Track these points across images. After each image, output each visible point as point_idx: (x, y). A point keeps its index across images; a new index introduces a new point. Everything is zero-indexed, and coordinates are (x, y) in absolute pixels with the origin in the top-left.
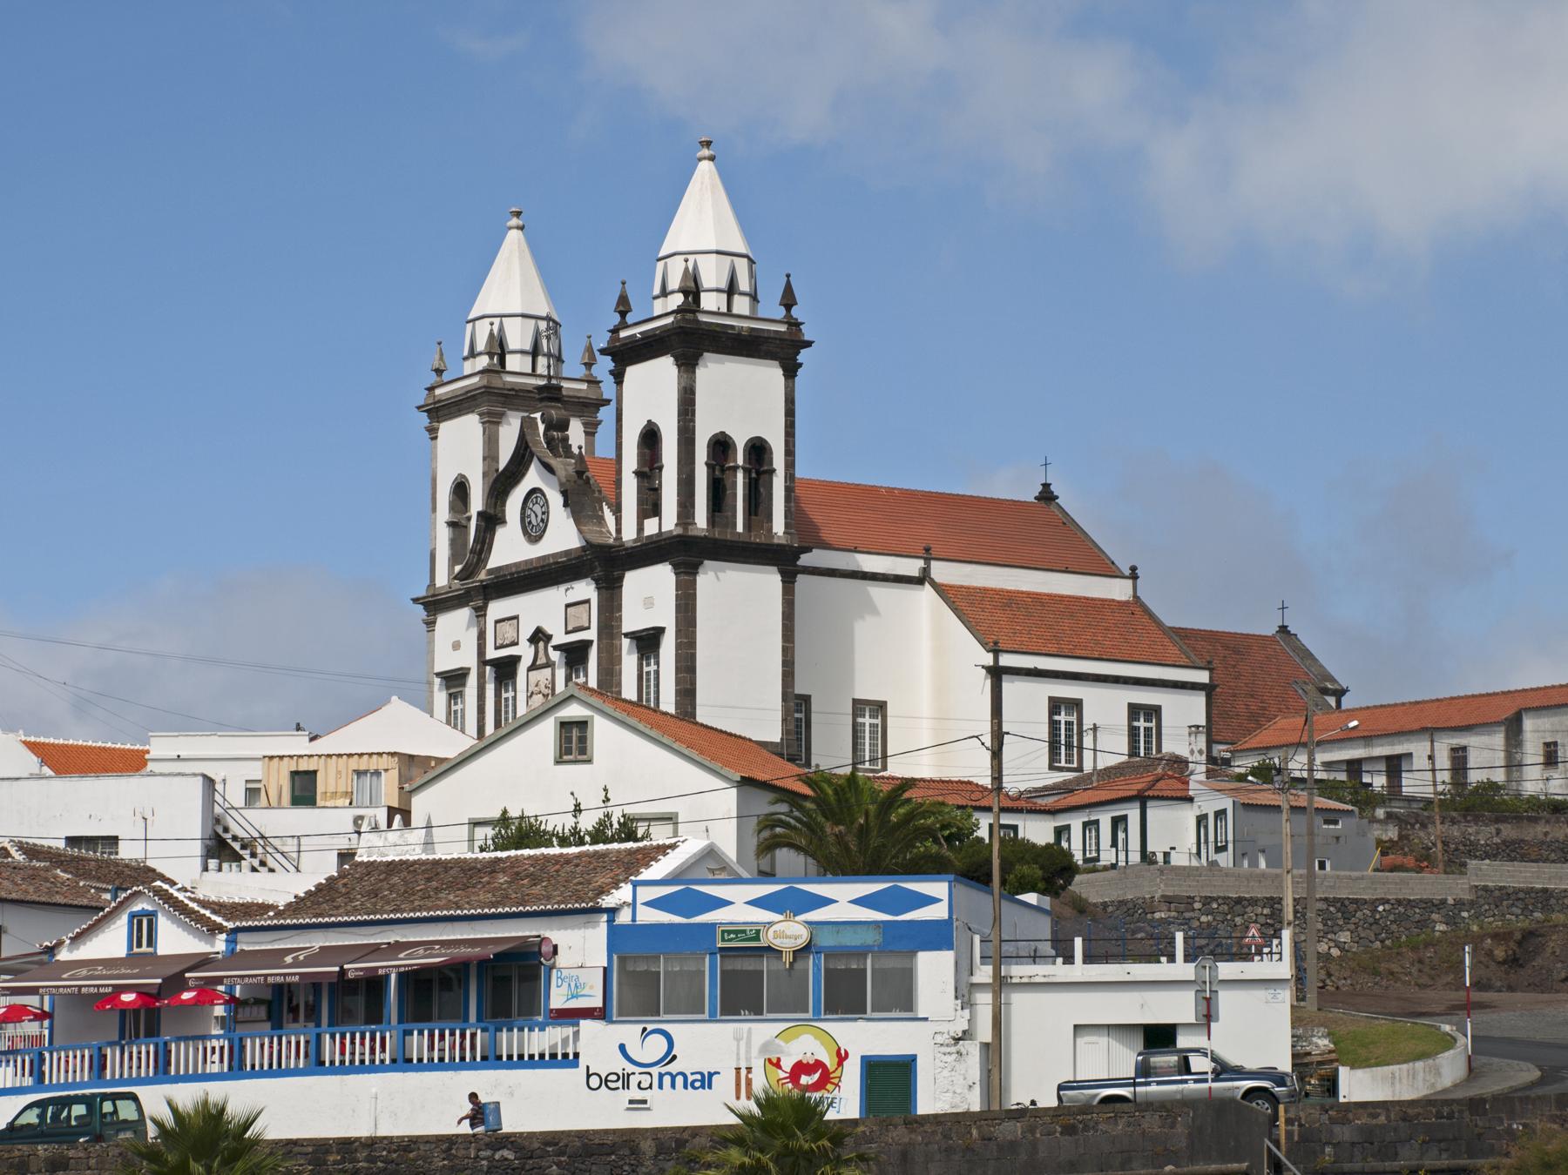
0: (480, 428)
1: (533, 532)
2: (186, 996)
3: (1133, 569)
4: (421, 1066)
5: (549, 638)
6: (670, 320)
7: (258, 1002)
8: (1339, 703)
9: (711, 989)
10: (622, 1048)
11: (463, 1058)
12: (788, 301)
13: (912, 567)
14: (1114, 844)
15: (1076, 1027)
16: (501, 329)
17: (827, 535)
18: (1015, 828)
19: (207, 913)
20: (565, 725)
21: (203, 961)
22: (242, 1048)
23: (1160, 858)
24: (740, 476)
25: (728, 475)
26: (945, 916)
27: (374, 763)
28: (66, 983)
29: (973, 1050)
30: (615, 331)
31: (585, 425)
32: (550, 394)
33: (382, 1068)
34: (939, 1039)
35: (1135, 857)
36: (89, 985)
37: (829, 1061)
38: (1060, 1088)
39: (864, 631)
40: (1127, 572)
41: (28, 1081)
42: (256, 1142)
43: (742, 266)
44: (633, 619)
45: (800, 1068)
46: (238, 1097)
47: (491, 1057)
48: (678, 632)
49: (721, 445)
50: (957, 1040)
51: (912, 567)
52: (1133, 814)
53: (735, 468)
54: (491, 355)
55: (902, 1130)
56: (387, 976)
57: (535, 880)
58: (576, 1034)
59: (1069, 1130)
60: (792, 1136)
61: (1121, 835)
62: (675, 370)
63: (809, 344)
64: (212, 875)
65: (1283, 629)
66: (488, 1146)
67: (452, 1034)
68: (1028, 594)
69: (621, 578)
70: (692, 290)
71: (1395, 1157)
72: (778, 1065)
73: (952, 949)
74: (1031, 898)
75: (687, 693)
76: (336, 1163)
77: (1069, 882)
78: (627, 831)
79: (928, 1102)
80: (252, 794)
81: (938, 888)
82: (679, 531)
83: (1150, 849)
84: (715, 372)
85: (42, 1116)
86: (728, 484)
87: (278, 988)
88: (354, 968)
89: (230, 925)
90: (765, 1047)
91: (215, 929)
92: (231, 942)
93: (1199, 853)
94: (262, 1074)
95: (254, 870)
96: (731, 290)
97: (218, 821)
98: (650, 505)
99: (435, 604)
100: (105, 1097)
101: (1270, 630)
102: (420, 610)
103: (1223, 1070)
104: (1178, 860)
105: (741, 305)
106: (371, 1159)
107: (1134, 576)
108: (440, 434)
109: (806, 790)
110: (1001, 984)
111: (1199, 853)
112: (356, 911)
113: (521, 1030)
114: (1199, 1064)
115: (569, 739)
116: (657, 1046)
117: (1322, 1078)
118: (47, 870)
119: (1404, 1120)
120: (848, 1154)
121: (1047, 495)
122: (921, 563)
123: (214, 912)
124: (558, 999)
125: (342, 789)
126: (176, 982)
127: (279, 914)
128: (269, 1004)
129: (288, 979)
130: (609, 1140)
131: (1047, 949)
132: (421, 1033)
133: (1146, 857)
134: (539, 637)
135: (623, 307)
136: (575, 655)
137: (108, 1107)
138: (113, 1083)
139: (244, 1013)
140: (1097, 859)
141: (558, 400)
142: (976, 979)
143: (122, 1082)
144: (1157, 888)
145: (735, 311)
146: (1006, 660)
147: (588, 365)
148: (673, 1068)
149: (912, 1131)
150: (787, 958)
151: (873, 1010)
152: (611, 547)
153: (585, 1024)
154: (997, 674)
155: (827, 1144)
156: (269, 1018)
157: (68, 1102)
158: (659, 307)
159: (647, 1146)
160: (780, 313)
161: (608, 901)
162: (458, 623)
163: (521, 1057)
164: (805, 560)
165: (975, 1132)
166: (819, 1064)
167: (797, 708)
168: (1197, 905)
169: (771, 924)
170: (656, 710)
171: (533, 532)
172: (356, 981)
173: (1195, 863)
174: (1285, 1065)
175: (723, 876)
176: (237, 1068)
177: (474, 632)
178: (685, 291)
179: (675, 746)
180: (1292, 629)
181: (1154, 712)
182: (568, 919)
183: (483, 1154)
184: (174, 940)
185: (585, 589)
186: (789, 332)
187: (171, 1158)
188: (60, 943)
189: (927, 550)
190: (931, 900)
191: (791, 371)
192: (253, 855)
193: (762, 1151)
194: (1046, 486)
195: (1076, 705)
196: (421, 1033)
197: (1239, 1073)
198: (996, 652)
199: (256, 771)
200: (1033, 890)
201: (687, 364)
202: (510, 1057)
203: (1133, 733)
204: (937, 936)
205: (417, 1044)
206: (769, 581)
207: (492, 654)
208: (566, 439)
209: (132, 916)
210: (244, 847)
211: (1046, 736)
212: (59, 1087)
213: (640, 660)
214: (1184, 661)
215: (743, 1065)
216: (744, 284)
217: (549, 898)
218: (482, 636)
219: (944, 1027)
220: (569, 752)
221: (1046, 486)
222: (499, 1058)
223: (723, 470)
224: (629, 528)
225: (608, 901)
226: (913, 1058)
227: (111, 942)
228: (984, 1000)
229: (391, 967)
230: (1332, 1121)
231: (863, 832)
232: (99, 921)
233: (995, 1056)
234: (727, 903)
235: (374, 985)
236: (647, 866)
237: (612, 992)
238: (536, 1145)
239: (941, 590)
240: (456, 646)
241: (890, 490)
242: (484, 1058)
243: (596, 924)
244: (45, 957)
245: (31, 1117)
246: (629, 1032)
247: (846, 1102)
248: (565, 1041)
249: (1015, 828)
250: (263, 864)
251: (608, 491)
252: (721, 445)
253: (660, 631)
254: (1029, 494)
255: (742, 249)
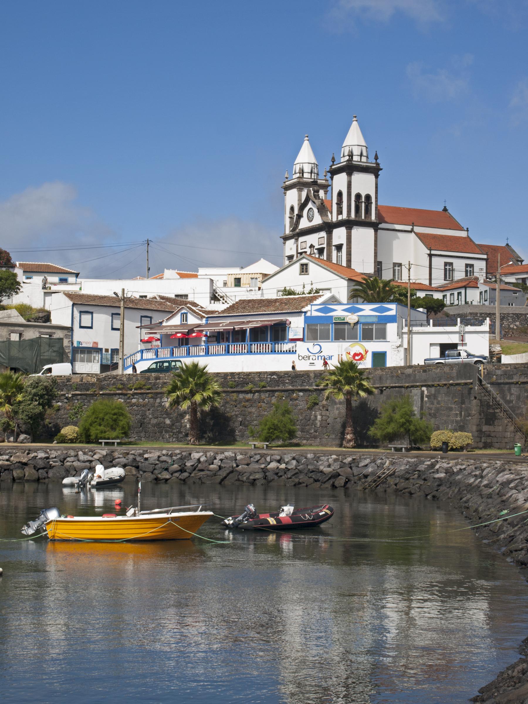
0: (297, 192)
1: (310, 219)
2: (194, 334)
3: (467, 229)
4: (255, 353)
5: (314, 247)
6: (345, 163)
7: (214, 336)
8: (521, 264)
9: (332, 334)
10: (308, 349)
11: (266, 352)
12: (376, 158)
13: (409, 228)
14: (458, 299)
15: (431, 344)
16: (303, 167)
17: (386, 219)
18: (432, 295)
19: (201, 313)
20: (302, 265)
21: (199, 326)
22: (209, 348)
23: (470, 303)
24: (363, 204)
25: (360, 204)
26: (395, 314)
27: (256, 276)
28: (164, 331)
29: (402, 350)
30: (331, 166)
31: (325, 191)
32: (314, 183)
33: (245, 354)
34: (393, 347)
35: (463, 303)
36: (169, 332)
37: (363, 353)
38: (425, 360)
39: (396, 244)
40: (466, 229)
41: (154, 357)
42: (206, 373)
43: (364, 149)
44: (336, 241)
45: (355, 355)
46: (202, 361)
47: (273, 351)
48: (347, 245)
49: (358, 196)
50: (398, 347)
51: (409, 228)
52: (463, 291)
53: (362, 202)
54: (300, 173)
55: (380, 371)
56: (246, 330)
57: (286, 304)
58: (296, 345)
59: (425, 371)
60: (348, 372)
61: (460, 297)
62: (346, 176)
63: (381, 169)
64: (212, 305)
65: (507, 245)
66: (270, 375)
67: (263, 345)
68: (440, 235)
69: (332, 231)
70: (351, 155)
71: (512, 379)
72: (349, 354)
73: (396, 322)
74: (421, 310)
75: (349, 261)
76: (230, 379)
77: (443, 309)
78: (317, 292)
79: (390, 363)
80: (225, 284)
81: (393, 306)
82: (347, 218)
83: (467, 300)
84: (357, 177)
85: (157, 366)
86: (360, 206)
87: (219, 333)
88: (237, 327)
89: (206, 316)
90: (346, 349)
91: (203, 317)
92: (207, 320)
93: (480, 302)
94: (213, 355)
95: (223, 303)
96: (361, 155)
97: (214, 290)
98: (340, 212)
99: (286, 238)
100: (172, 361)
101: (504, 245)
102: (282, 240)
103: (469, 355)
104: (474, 303)
105: (364, 159)
106: (239, 378)
107: (467, 230)
108: (287, 194)
109: (364, 282)
110: (410, 332)
111: (480, 302)
112: (239, 312)
113: (281, 344)
114: (463, 354)
115: (303, 269)
116: (317, 348)
117: (497, 358)
118: (164, 302)
119: (515, 368)
120: (364, 377)
121: (445, 210)
122: (411, 227)
123: (203, 313)
124: (291, 336)
125: (247, 282)
126: (191, 331)
127: (219, 313)
128: (216, 337)
129: (220, 330)
130: (302, 373)
131: (425, 323)
132: (255, 345)
133: (466, 303)
134: (312, 246)
135: (333, 160)
136: (321, 251)
137: (173, 364)
138: (176, 357)
139: (210, 339)
140: (453, 303)
141: (317, 185)
142: (403, 331)
143: (178, 357)
144: (468, 311)
145: (362, 161)
146: (433, 252)
147: (325, 176)
148: (322, 354)
149: (383, 371)
150: (352, 325)
151: (375, 339)
152: (330, 223)
153: (298, 343)
154: (430, 256)
155: (358, 374)
156: (216, 341)
157: (163, 362)
158: (343, 160)
159: (312, 375)
160: (374, 161)
161: (304, 310)
162: (291, 243)
163: (281, 351)
164: (380, 226)
165: (399, 372)
166: (360, 354)
167: (378, 265)
168: (478, 315)
169: (348, 316)
170: (341, 266)
171: (310, 219)
172: (238, 331)
173: (479, 304)
174: (487, 354)
175: (336, 303)
176: (207, 353)
177: (295, 245)
178: (349, 156)
179: (331, 270)
180: (510, 245)
181: (472, 266)
182: (294, 314)
183: (268, 377)
184: (192, 320)
185: (323, 234)
186: (376, 166)
187: (184, 376)
188: (163, 321)
189: (413, 223)
190: (390, 310)
191: (377, 176)
192: (223, 300)
193: (340, 376)
194: (445, 207)
195: (451, 264)
196: (255, 345)
197: (474, 356)
198: (430, 250)
199: (225, 278)
200: (422, 307)
201: (350, 175)
202: (278, 351)
203: (466, 271)
204: (392, 319)
205: (254, 347)
206: (371, 232)
207: (300, 251)
208: (318, 195)
209: (182, 314)
210: (221, 297)
211: (433, 269)
212: (162, 358)
213: (337, 252)
214: (480, 252)
215: (340, 354)
216: (365, 154)
217: (289, 309)
218: (297, 246)
219: (394, 344)
220: (303, 272)
221: (445, 207)
222: (275, 351)
223: (359, 203)
224: (334, 217)
225: (304, 310)
226: (386, 352)
227: (176, 321)
228: (405, 337)
229: (248, 327)
230: (496, 369)
231: (379, 293)
232: (171, 317)
233: (408, 352)
234: (335, 310)
235: (243, 332)
236: (316, 300)
237: (219, 320)
238: (282, 374)
239: (416, 234)
240: (291, 249)
241: (404, 208)
242: (271, 351)
243: (301, 316)
244: (159, 325)
245: (154, 366)
246: (310, 345)
247: (367, 364)
248: (293, 347)
249: (432, 295)
250: (226, 302)
251: (329, 208)
252: (358, 196)
253: (341, 245)
254: (441, 209)
255: (364, 145)
